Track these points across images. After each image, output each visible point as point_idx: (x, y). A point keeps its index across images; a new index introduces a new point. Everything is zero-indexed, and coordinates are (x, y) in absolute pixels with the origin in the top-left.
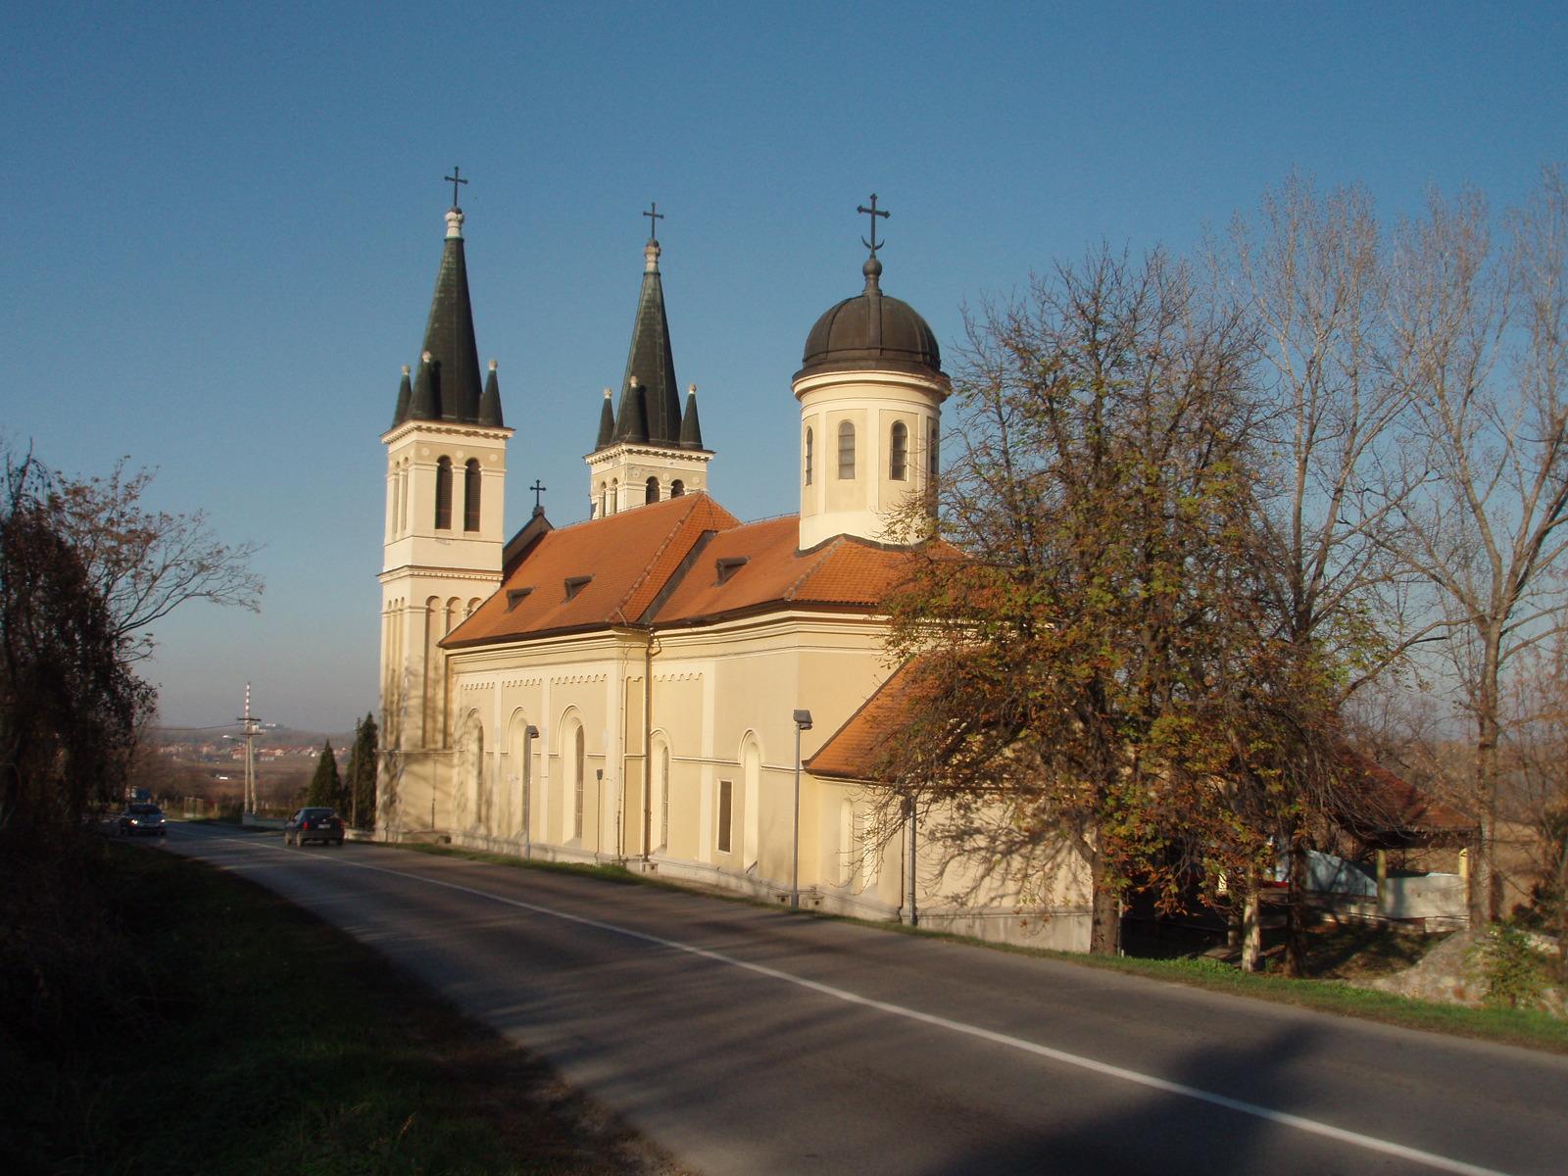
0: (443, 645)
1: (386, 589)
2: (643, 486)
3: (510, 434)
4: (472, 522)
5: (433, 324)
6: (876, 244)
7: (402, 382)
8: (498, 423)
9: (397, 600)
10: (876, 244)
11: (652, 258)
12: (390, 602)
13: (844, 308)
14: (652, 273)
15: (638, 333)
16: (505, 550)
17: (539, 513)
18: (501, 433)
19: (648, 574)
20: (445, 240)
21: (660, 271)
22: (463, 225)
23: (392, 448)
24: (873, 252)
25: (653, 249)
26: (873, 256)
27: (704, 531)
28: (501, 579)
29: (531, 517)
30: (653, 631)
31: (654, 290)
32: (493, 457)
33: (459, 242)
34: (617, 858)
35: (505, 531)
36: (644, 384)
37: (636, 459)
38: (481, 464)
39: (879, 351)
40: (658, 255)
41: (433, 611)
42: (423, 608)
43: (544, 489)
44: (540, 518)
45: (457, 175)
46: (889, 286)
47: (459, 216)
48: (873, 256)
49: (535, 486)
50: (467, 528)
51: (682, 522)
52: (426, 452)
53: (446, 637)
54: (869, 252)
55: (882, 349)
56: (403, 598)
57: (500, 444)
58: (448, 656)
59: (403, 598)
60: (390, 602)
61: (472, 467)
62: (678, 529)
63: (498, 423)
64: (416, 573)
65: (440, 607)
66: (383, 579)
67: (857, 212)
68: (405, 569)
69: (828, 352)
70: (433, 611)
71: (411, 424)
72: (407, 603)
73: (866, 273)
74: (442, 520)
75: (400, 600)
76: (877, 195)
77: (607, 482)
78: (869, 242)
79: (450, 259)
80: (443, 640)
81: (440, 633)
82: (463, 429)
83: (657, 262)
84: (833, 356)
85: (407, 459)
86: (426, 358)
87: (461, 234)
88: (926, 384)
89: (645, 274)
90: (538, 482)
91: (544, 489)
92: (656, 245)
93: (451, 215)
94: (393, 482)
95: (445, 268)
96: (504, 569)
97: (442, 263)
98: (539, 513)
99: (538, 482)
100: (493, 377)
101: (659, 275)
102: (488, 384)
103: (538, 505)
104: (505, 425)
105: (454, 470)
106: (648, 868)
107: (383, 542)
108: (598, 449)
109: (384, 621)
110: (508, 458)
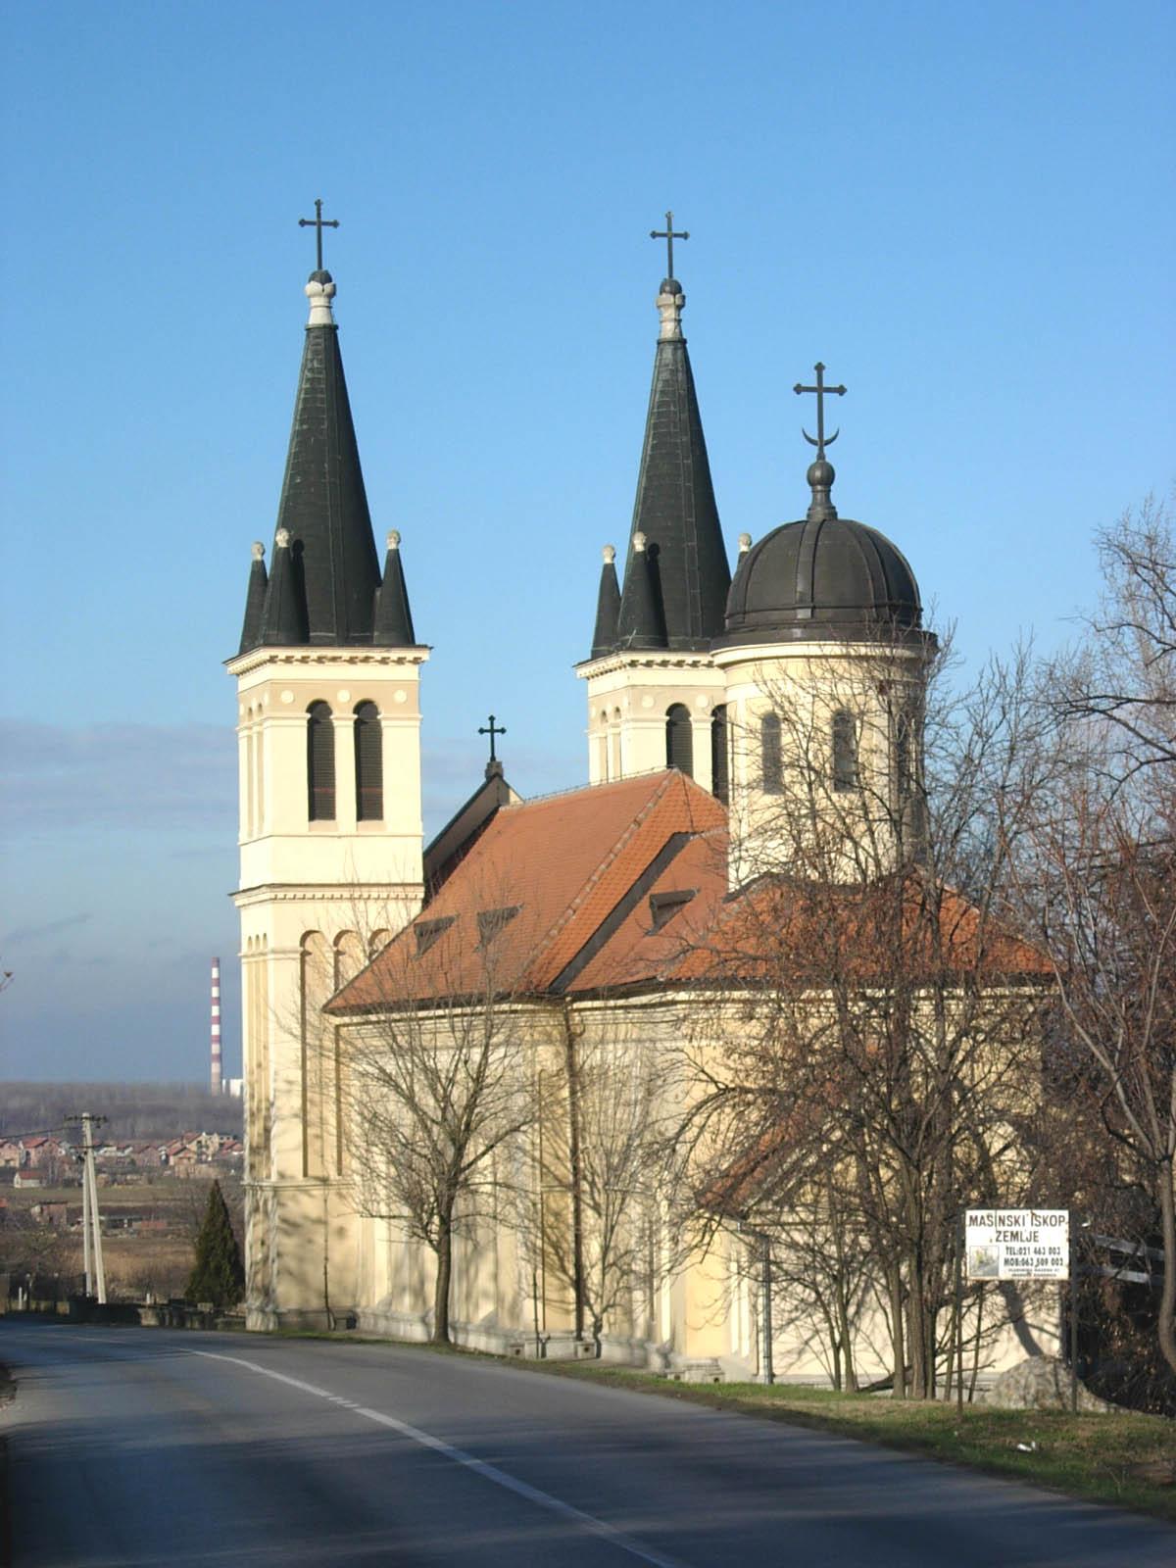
0: (329, 1009)
1: (245, 914)
2: (661, 720)
3: (425, 655)
4: (369, 806)
5: (293, 477)
6: (826, 438)
7: (253, 572)
8: (407, 638)
9: (258, 937)
10: (826, 438)
11: (670, 313)
12: (250, 938)
13: (769, 545)
14: (669, 342)
15: (649, 452)
16: (426, 855)
17: (494, 774)
18: (410, 654)
19: (575, 912)
20: (308, 330)
21: (685, 337)
22: (333, 300)
23: (244, 683)
24: (821, 450)
25: (669, 299)
26: (821, 456)
27: (674, 834)
28: (422, 895)
29: (484, 780)
30: (574, 1001)
31: (674, 372)
32: (400, 696)
33: (330, 332)
34: (762, 1378)
35: (427, 811)
36: (656, 541)
37: (641, 676)
38: (381, 709)
39: (810, 611)
40: (679, 308)
41: (310, 954)
42: (295, 952)
43: (503, 731)
44: (497, 779)
45: (319, 215)
46: (849, 505)
47: (328, 287)
48: (821, 456)
49: (487, 727)
50: (361, 816)
51: (638, 823)
52: (287, 697)
53: (335, 997)
54: (815, 449)
55: (814, 608)
56: (265, 935)
57: (410, 672)
58: (337, 1027)
59: (265, 935)
60: (250, 938)
61: (366, 715)
62: (631, 835)
63: (407, 638)
64: (281, 895)
65: (324, 953)
66: (240, 901)
67: (794, 394)
68: (263, 889)
69: (745, 613)
70: (310, 954)
71: (264, 654)
72: (271, 944)
73: (812, 482)
74: (320, 806)
75: (261, 937)
76: (824, 364)
77: (608, 713)
78: (815, 437)
79: (316, 365)
80: (330, 1002)
81: (323, 992)
82: (346, 653)
83: (679, 321)
84: (752, 618)
85: (260, 706)
86: (282, 539)
87: (331, 316)
88: (878, 652)
89: (659, 343)
90: (492, 719)
91: (503, 731)
92: (677, 289)
93: (314, 287)
94: (246, 739)
95: (308, 380)
96: (426, 879)
97: (303, 372)
98: (494, 774)
99: (492, 719)
100: (395, 558)
101: (684, 342)
102: (388, 561)
103: (493, 758)
104: (417, 642)
105: (336, 723)
106: (580, 1350)
107: (238, 840)
108: (596, 655)
109: (245, 969)
110: (424, 698)
